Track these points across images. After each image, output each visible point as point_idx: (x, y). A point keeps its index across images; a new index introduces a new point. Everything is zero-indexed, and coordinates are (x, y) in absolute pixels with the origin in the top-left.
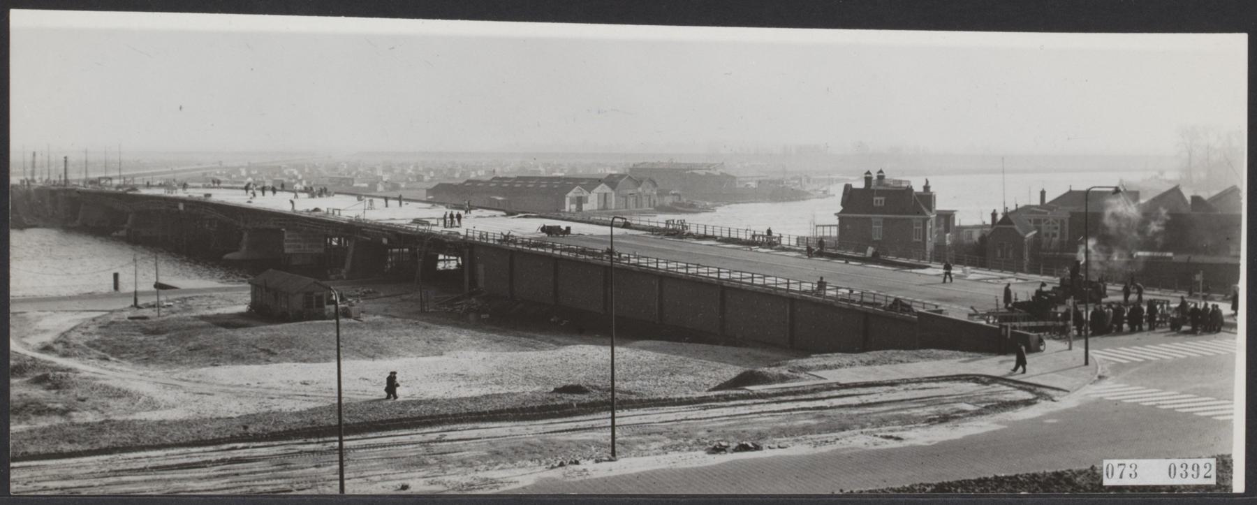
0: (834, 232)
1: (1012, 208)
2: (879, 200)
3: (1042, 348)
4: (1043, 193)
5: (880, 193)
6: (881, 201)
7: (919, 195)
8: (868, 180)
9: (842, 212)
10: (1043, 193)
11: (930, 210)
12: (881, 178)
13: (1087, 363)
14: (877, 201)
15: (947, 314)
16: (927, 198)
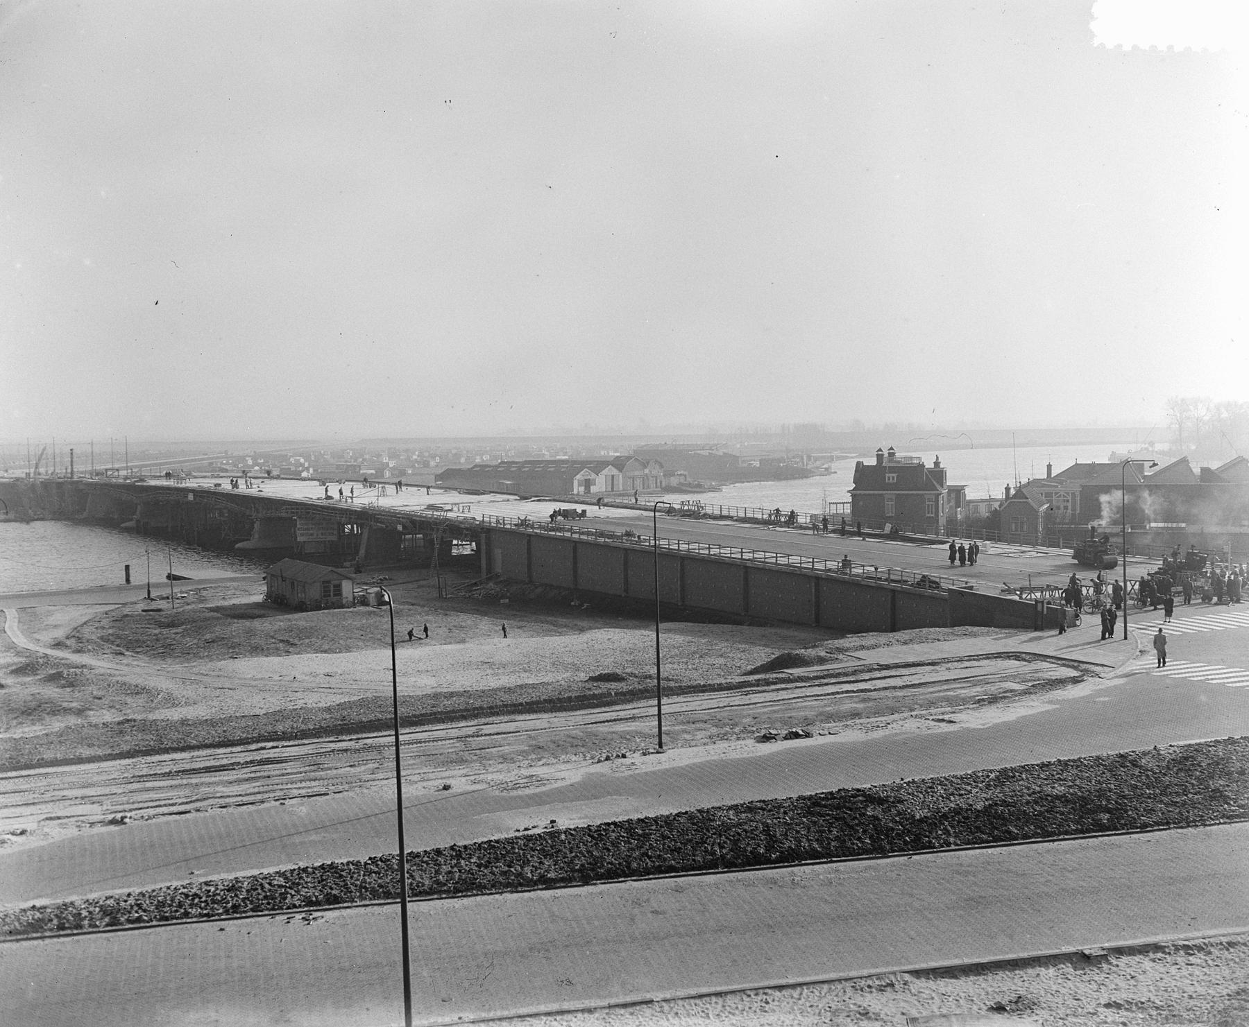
0: (848, 510)
1: (1024, 481)
2: (891, 477)
3: (1078, 623)
4: (1049, 467)
5: (892, 470)
6: (893, 478)
7: (930, 471)
8: (880, 457)
9: (853, 490)
10: (1049, 467)
11: (942, 486)
12: (891, 455)
13: (1126, 638)
14: (889, 478)
15: (977, 590)
16: (938, 474)
